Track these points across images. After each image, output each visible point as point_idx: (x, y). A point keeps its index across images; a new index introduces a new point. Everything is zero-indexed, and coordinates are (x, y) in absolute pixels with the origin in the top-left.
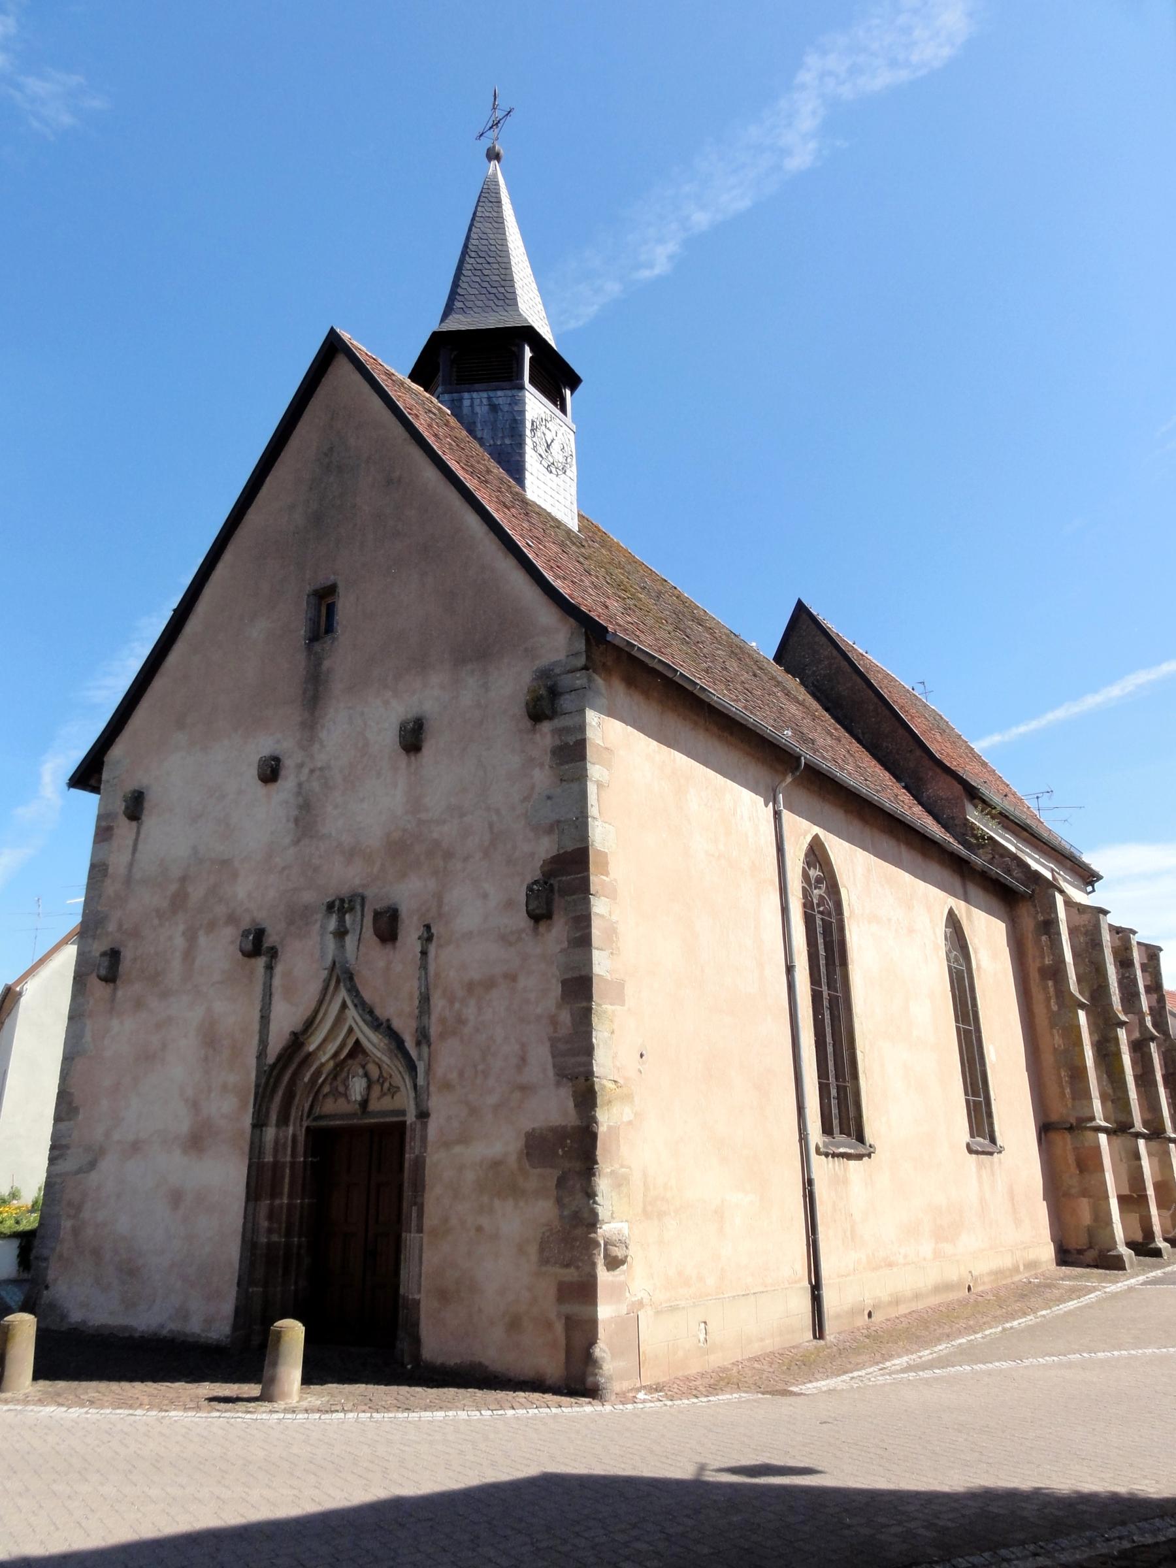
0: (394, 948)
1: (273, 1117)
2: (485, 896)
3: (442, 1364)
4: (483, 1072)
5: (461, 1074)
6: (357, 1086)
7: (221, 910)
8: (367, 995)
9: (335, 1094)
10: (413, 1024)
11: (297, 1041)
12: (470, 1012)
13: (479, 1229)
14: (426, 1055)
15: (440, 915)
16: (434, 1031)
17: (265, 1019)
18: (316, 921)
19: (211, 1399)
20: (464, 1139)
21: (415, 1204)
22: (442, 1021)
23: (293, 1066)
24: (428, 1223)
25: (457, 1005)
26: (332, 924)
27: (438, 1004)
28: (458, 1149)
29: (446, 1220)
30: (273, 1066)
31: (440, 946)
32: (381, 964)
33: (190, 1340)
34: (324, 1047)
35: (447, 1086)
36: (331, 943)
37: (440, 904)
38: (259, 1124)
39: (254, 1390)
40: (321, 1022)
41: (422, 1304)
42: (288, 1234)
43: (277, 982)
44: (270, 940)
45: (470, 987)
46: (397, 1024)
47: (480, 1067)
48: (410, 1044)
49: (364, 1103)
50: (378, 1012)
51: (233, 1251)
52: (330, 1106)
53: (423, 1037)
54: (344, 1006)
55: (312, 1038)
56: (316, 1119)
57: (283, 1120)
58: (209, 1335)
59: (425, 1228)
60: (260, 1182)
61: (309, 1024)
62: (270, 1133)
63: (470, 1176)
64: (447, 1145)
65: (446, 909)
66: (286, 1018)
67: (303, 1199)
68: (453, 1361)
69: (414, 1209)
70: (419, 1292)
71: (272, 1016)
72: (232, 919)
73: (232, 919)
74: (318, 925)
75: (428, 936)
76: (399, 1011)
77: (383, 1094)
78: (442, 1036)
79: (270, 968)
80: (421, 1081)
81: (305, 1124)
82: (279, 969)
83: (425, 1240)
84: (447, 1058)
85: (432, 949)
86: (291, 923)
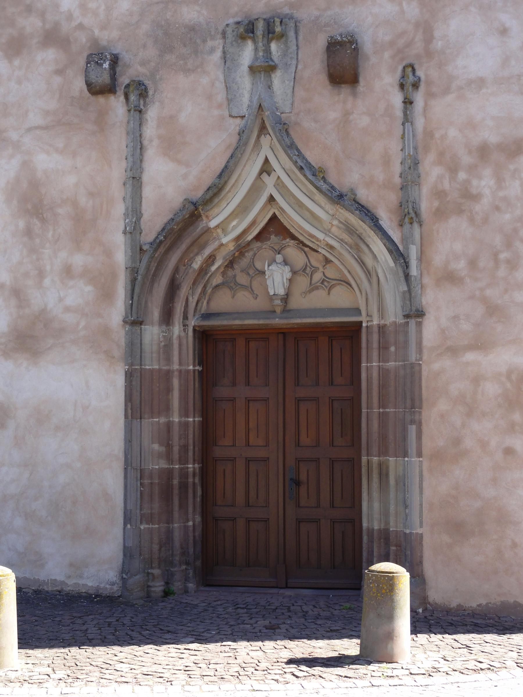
0: (355, 95)
1: (156, 313)
2: (504, 31)
3: (459, 606)
4: (508, 262)
5: (473, 263)
6: (277, 279)
7: (31, 24)
8: (313, 156)
9: (230, 285)
10: (393, 198)
11: (190, 217)
12: (485, 183)
13: (509, 451)
14: (417, 237)
15: (429, 54)
16: (426, 206)
17: (135, 180)
18: (212, 50)
19: (291, 662)
20: (480, 344)
21: (412, 422)
22: (440, 194)
23: (183, 247)
24: (427, 444)
25: (462, 175)
26: (247, 54)
27: (432, 173)
28: (470, 356)
29: (457, 441)
30: (157, 244)
31: (430, 95)
32: (333, 115)
33: (49, 588)
34: (229, 223)
35: (450, 278)
36: (245, 83)
37: (429, 39)
38: (135, 321)
39: (350, 647)
40: (229, 191)
41: (427, 541)
42: (183, 460)
43: (150, 130)
44: (133, 69)
45: (483, 152)
46: (364, 195)
47: (503, 256)
48: (387, 221)
49: (286, 299)
50: (332, 179)
51: (112, 481)
52: (223, 301)
53: (409, 214)
54: (266, 168)
55: (216, 211)
56: (207, 316)
57: (167, 317)
58: (81, 582)
59: (425, 451)
60: (141, 396)
61: (215, 191)
62: (152, 333)
63: (491, 389)
64: (453, 351)
65: (439, 44)
66: (167, 183)
67: (194, 417)
68: (473, 603)
69: (414, 427)
70: (421, 526)
71: (145, 178)
72: (52, 37)
73: (52, 37)
74: (218, 53)
75: (409, 82)
76: (371, 178)
77: (313, 288)
78: (440, 214)
79: (138, 112)
80: (414, 271)
81: (192, 322)
82: (152, 114)
83: (426, 466)
84: (449, 243)
85: (419, 98)
86: (166, 49)
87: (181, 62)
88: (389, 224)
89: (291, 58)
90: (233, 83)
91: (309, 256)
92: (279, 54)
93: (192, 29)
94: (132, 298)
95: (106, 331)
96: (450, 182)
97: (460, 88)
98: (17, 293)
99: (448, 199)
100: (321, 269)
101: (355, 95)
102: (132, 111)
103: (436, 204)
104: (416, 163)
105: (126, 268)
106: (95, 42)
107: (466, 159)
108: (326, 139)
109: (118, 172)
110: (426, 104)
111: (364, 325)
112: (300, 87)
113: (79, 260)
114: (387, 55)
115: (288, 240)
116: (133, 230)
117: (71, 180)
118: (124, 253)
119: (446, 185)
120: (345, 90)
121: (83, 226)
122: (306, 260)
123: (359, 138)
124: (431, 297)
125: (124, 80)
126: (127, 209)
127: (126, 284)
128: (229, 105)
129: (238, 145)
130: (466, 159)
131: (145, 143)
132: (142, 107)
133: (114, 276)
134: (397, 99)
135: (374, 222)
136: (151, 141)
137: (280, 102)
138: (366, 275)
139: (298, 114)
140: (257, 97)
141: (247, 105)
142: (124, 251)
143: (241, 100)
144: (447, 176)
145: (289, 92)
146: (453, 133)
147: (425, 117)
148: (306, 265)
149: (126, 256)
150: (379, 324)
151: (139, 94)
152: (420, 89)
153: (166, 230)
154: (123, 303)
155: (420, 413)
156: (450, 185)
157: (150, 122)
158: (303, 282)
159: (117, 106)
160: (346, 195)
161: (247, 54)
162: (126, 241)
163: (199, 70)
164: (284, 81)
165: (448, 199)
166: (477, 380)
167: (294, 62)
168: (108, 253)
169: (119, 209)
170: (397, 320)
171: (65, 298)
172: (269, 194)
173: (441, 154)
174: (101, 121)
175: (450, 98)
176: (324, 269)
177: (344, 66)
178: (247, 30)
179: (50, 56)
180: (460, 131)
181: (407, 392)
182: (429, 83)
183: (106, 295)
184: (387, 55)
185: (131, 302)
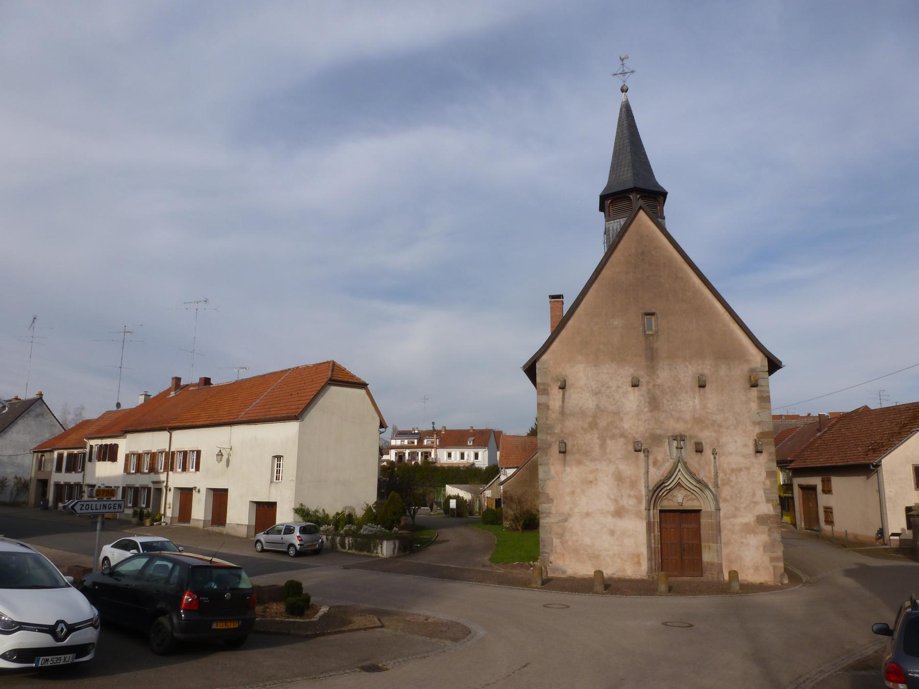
5: (731, 497)
10: (713, 481)
12: (733, 478)
13: (742, 543)
16: (720, 483)
17: (647, 472)
20: (734, 516)
22: (723, 480)
27: (721, 475)
35: (726, 500)
36: (675, 450)
43: (651, 461)
45: (733, 470)
48: (711, 487)
53: (716, 485)
66: (656, 475)
72: (622, 435)
73: (622, 435)
78: (723, 485)
82: (650, 457)
93: (660, 436)
95: (640, 511)
98: (616, 501)
106: (634, 437)
107: (729, 472)
109: (642, 471)
112: (688, 453)
113: (632, 493)
116: (647, 487)
117: (629, 472)
121: (633, 484)
123: (704, 467)
124: (721, 505)
130: (729, 472)
134: (712, 457)
135: (707, 487)
151: (647, 452)
155: (772, 560)
158: (686, 499)
159: (641, 454)
160: (583, 491)
161: (675, 443)
166: (734, 525)
168: (640, 491)
169: (643, 480)
171: (628, 503)
174: (637, 458)
177: (699, 450)
178: (675, 438)
179: (622, 440)
181: (718, 528)
183: (640, 502)
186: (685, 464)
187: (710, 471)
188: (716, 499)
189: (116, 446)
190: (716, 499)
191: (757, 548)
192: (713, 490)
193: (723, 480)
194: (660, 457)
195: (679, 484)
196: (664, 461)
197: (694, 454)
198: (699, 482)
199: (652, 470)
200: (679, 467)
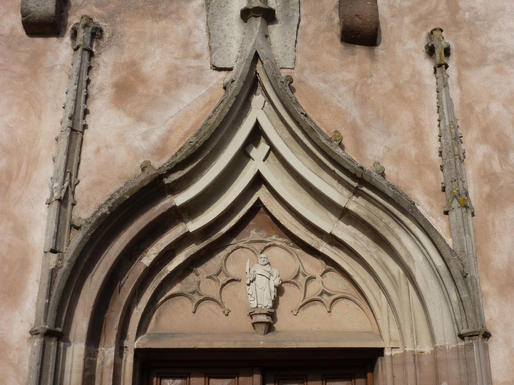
0: (373, 57)
10: (434, 178)
16: (475, 192)
17: (76, 130)
22: (487, 176)
27: (478, 154)
31: (463, 65)
43: (103, 76)
48: (426, 207)
53: (455, 197)
66: (123, 146)
78: (493, 201)
87: (151, 7)
88: (428, 209)
89: (294, 10)
90: (218, 30)
91: (302, 260)
92: (278, 4)
94: (49, 296)
96: (501, 163)
97: (497, 62)
99: (501, 184)
100: (319, 278)
101: (373, 57)
102: (80, 50)
103: (487, 189)
104: (458, 139)
105: (45, 252)
108: (340, 102)
109: (53, 123)
110: (460, 74)
111: (387, 353)
114: (407, 20)
115: (274, 237)
118: (44, 232)
119: (497, 167)
120: (360, 51)
122: (299, 264)
125: (73, 20)
126: (57, 171)
127: (42, 275)
128: (211, 55)
129: (224, 97)
131: (93, 91)
132: (94, 50)
133: (25, 263)
134: (427, 66)
135: (401, 206)
136: (101, 89)
137: (280, 55)
138: (392, 283)
139: (302, 70)
140: (252, 44)
141: (235, 57)
142: (45, 228)
143: (228, 50)
144: (496, 156)
145: (292, 44)
146: (495, 108)
147: (461, 88)
148: (299, 272)
149: (47, 235)
150: (414, 351)
152: (451, 57)
153: (113, 200)
154: (34, 304)
156: (501, 167)
157: (102, 67)
159: (61, 51)
162: (49, 215)
163: (173, 16)
164: (285, 34)
165: (501, 184)
167: (297, 15)
168: (20, 231)
170: (447, 343)
172: (257, 170)
173: (485, 131)
174: (35, 64)
175: (487, 70)
176: (323, 278)
180: (504, 106)
182: (461, 52)
184: (407, 20)
185: (47, 301)
186: (285, 88)
187: (419, 135)
188: (459, 275)
189: (138, 352)
190: (459, 275)
191: (49, 203)
192: (440, 224)
193: (487, 176)
194: (156, 63)
195: (250, 215)
196: (175, 82)
197: (332, 51)
198: (360, 181)
199: (105, 122)
200: (258, 111)
